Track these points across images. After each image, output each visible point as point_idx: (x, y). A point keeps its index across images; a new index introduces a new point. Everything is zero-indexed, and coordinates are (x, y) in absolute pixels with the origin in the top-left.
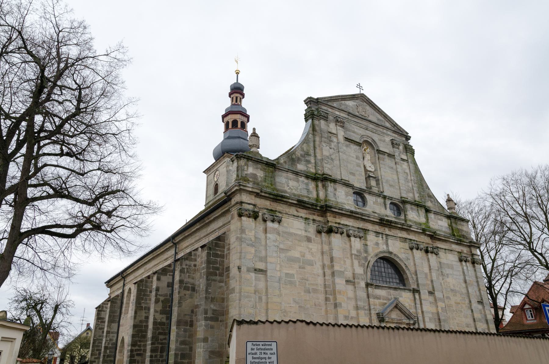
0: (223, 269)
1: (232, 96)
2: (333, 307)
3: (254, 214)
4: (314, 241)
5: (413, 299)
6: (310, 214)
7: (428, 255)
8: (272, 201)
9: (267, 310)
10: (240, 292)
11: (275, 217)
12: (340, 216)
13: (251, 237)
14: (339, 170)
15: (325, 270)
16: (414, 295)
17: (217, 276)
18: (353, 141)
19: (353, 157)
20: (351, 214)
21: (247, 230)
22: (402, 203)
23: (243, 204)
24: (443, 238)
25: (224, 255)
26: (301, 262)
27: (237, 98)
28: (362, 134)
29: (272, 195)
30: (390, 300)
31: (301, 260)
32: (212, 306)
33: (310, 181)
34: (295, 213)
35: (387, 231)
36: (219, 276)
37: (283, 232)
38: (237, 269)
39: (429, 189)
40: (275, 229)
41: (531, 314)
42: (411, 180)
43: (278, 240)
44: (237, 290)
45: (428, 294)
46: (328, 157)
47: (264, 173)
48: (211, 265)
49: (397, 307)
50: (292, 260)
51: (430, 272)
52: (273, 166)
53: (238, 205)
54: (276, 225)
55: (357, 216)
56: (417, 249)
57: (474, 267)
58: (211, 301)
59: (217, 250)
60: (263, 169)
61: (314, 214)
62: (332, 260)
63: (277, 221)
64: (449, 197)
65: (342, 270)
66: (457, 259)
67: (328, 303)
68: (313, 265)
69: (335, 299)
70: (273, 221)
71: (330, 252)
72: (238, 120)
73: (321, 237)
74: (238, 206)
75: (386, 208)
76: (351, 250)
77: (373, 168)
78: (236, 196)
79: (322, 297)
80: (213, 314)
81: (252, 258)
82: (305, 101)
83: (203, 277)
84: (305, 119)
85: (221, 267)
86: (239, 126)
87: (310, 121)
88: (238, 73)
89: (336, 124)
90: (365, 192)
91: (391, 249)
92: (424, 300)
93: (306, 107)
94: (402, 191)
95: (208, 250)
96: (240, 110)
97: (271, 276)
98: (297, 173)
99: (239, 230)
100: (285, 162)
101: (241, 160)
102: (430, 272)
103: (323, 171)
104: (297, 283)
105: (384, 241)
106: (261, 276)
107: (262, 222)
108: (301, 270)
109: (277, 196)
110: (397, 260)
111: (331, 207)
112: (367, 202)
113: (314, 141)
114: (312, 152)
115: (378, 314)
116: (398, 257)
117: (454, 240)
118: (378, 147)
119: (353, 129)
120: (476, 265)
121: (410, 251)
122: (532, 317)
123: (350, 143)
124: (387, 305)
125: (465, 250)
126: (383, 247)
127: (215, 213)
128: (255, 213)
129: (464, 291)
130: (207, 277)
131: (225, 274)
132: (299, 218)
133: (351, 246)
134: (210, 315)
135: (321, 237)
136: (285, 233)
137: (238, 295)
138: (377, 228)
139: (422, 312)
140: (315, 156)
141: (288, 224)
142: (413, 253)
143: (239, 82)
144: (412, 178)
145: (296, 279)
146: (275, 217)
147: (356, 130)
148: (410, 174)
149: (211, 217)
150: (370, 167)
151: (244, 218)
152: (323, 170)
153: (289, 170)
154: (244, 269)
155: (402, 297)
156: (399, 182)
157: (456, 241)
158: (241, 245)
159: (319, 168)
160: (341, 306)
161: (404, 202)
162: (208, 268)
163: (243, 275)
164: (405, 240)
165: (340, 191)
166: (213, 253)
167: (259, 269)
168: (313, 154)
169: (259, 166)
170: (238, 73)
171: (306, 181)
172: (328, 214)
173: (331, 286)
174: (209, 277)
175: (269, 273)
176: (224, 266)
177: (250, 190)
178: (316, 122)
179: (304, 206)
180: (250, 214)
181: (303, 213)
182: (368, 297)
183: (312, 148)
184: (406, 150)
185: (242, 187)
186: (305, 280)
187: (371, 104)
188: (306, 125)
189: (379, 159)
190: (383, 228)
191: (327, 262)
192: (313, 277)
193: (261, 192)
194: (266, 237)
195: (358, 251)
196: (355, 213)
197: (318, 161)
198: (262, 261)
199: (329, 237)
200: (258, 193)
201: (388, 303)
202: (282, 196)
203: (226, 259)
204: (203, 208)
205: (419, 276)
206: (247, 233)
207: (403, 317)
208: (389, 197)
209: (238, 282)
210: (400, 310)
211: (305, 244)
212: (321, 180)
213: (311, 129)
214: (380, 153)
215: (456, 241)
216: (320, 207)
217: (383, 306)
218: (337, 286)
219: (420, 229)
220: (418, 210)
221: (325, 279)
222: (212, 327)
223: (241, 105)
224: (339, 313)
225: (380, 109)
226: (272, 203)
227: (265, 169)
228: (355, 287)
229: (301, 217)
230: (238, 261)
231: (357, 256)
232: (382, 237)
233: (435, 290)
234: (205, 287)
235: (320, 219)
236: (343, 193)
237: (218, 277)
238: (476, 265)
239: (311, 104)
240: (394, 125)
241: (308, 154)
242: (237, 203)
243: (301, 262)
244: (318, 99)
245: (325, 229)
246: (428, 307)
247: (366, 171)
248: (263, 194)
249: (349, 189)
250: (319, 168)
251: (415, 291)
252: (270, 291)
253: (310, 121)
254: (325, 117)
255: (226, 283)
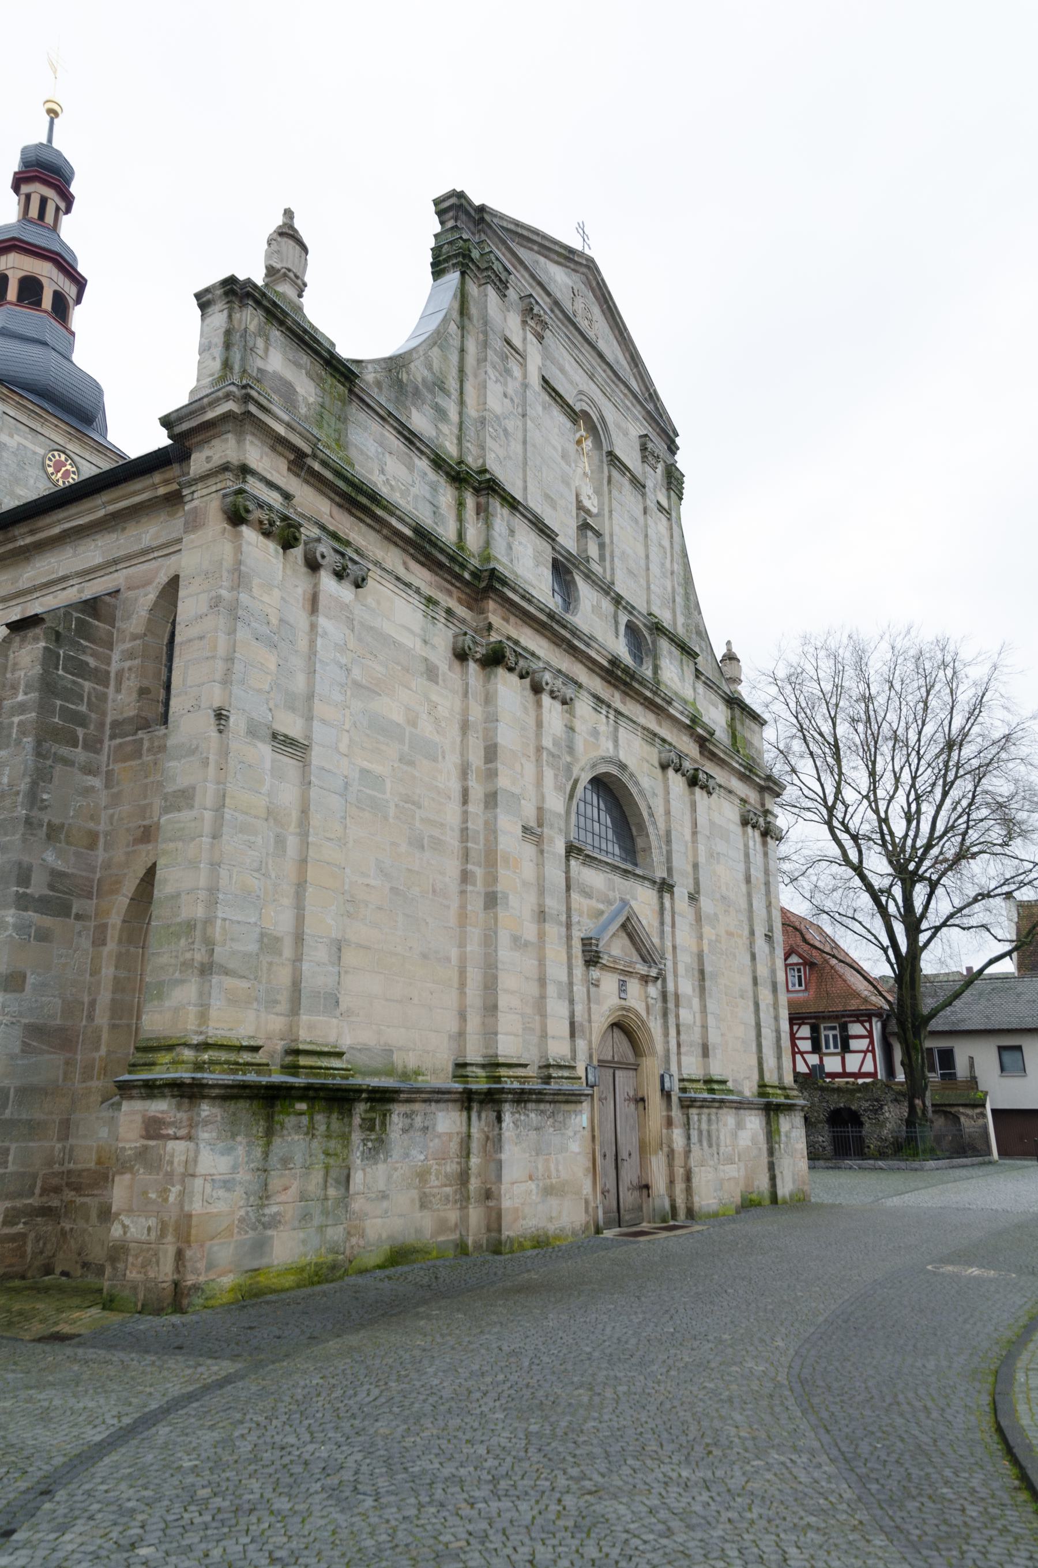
0: (102, 725)
1: (25, 189)
2: (482, 905)
3: (283, 529)
4: (444, 681)
5: (657, 908)
6: (441, 589)
7: (693, 793)
8: (340, 506)
9: (301, 886)
10: (219, 808)
11: (350, 564)
12: (519, 622)
13: (269, 610)
14: (521, 476)
15: (470, 783)
16: (661, 898)
17: (76, 746)
18: (560, 396)
19: (554, 448)
20: (549, 622)
21: (256, 582)
22: (650, 629)
23: (250, 479)
24: (722, 755)
25: (108, 673)
26: (407, 741)
27: (44, 201)
28: (581, 387)
29: (345, 479)
30: (612, 905)
31: (407, 734)
32: (50, 857)
33: (441, 480)
34: (401, 572)
35: (616, 700)
36: (87, 747)
37: (361, 623)
38: (212, 720)
39: (700, 613)
40: (345, 607)
41: (800, 977)
42: (672, 573)
43: (351, 646)
44: (207, 795)
45: (687, 898)
46: (497, 417)
47: (318, 390)
48: (59, 702)
49: (629, 929)
50: (382, 728)
51: (694, 841)
52: (347, 378)
53: (228, 475)
54: (344, 592)
55: (563, 632)
56: (677, 771)
57: (765, 844)
58: (49, 837)
59: (84, 650)
60: (314, 376)
61: (450, 593)
62: (491, 753)
63: (352, 577)
64: (729, 650)
65: (516, 790)
66: (737, 819)
67: (470, 888)
68: (435, 760)
69: (492, 878)
70: (340, 575)
71: (485, 729)
72: (45, 282)
73: (465, 673)
74: (231, 483)
75: (617, 636)
76: (539, 735)
77: (596, 503)
78: (215, 442)
79: (452, 867)
80: (51, 887)
81: (267, 688)
82: (437, 202)
83: (18, 742)
84: (433, 265)
85: (93, 716)
86: (47, 302)
87: (453, 278)
88: (57, 114)
89: (524, 322)
90: (577, 568)
91: (623, 757)
92: (323, 721)
93: (438, 228)
94: (653, 596)
95: (47, 640)
96: (57, 248)
97: (323, 768)
98: (410, 438)
99: (225, 574)
100: (379, 384)
101: (245, 305)
102: (694, 841)
103: (480, 461)
104: (392, 811)
105: (611, 729)
106: (289, 764)
107: (304, 569)
108: (405, 768)
109: (359, 487)
110: (634, 790)
111: (504, 582)
112: (577, 600)
113: (462, 350)
114: (452, 384)
115: (586, 942)
116: (637, 783)
117: (740, 765)
118: (611, 444)
119: (561, 361)
120: (769, 839)
121: (659, 771)
122: (800, 985)
123: (552, 402)
124: (606, 916)
125: (753, 796)
126: (606, 747)
127: (73, 510)
128: (290, 526)
129: (743, 904)
130: (39, 743)
131: (106, 743)
132: (410, 592)
133: (539, 724)
134: (38, 888)
135: (465, 673)
136: (371, 629)
137: (208, 815)
138: (595, 684)
139: (674, 947)
140: (462, 403)
141: (378, 603)
142: (666, 780)
143: (56, 145)
144: (676, 567)
145: (388, 796)
146: (350, 564)
147: (567, 367)
148: (672, 555)
149: (50, 526)
150: (590, 498)
151: (249, 534)
152: (484, 457)
153: (390, 414)
154: (236, 722)
155: (636, 899)
156: (648, 569)
157: (742, 770)
158: (232, 632)
159: (469, 445)
160: (507, 904)
161: (658, 629)
162: (44, 708)
163: (234, 746)
164: (652, 737)
165: (524, 540)
166: (68, 658)
167: (285, 736)
168: (455, 395)
169: (305, 359)
170: (53, 113)
171: (432, 475)
172: (491, 605)
173: (482, 837)
174: (46, 745)
175: (317, 756)
176: (104, 714)
177: (281, 430)
178: (473, 289)
179: (428, 555)
180: (272, 523)
181: (421, 577)
182: (568, 888)
183: (454, 372)
184: (669, 483)
185: (253, 409)
186: (413, 803)
187: (606, 302)
188: (433, 288)
189: (609, 482)
190: (611, 689)
191: (476, 759)
192: (433, 799)
193: (314, 456)
194: (313, 627)
195: (555, 743)
196: (558, 622)
197: (468, 423)
198: (293, 709)
199: (488, 679)
200: (304, 455)
201: (609, 911)
202: (374, 497)
203: (118, 690)
204: (184, 400)
205: (675, 846)
206: (256, 591)
207: (636, 958)
208: (628, 603)
209: (212, 770)
210: (630, 936)
211: (419, 682)
212: (474, 488)
213: (456, 305)
214: (615, 466)
215: (742, 770)
216: (473, 574)
217: (596, 918)
218: (501, 839)
219: (687, 717)
220: (682, 660)
221: (465, 813)
222: (44, 936)
223: (55, 228)
224: (499, 924)
225: (626, 329)
226: (336, 511)
227: (321, 379)
228: (542, 852)
229: (418, 591)
230: (217, 689)
231: (553, 756)
232: (607, 717)
233: (702, 891)
234: (28, 780)
235: (463, 615)
236: (530, 551)
237: (79, 750)
238: (769, 839)
239: (456, 219)
240: (650, 395)
241: (439, 385)
242: (225, 468)
243: (407, 741)
244: (482, 209)
245: (480, 651)
246: (684, 936)
247: (580, 507)
248: (317, 466)
249: (545, 544)
250: (469, 445)
251: (665, 887)
252: (316, 819)
253: (453, 278)
254: (501, 280)
255: (107, 779)
